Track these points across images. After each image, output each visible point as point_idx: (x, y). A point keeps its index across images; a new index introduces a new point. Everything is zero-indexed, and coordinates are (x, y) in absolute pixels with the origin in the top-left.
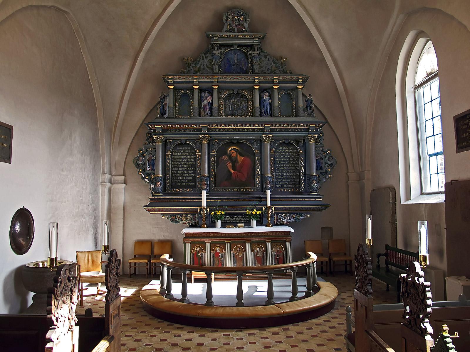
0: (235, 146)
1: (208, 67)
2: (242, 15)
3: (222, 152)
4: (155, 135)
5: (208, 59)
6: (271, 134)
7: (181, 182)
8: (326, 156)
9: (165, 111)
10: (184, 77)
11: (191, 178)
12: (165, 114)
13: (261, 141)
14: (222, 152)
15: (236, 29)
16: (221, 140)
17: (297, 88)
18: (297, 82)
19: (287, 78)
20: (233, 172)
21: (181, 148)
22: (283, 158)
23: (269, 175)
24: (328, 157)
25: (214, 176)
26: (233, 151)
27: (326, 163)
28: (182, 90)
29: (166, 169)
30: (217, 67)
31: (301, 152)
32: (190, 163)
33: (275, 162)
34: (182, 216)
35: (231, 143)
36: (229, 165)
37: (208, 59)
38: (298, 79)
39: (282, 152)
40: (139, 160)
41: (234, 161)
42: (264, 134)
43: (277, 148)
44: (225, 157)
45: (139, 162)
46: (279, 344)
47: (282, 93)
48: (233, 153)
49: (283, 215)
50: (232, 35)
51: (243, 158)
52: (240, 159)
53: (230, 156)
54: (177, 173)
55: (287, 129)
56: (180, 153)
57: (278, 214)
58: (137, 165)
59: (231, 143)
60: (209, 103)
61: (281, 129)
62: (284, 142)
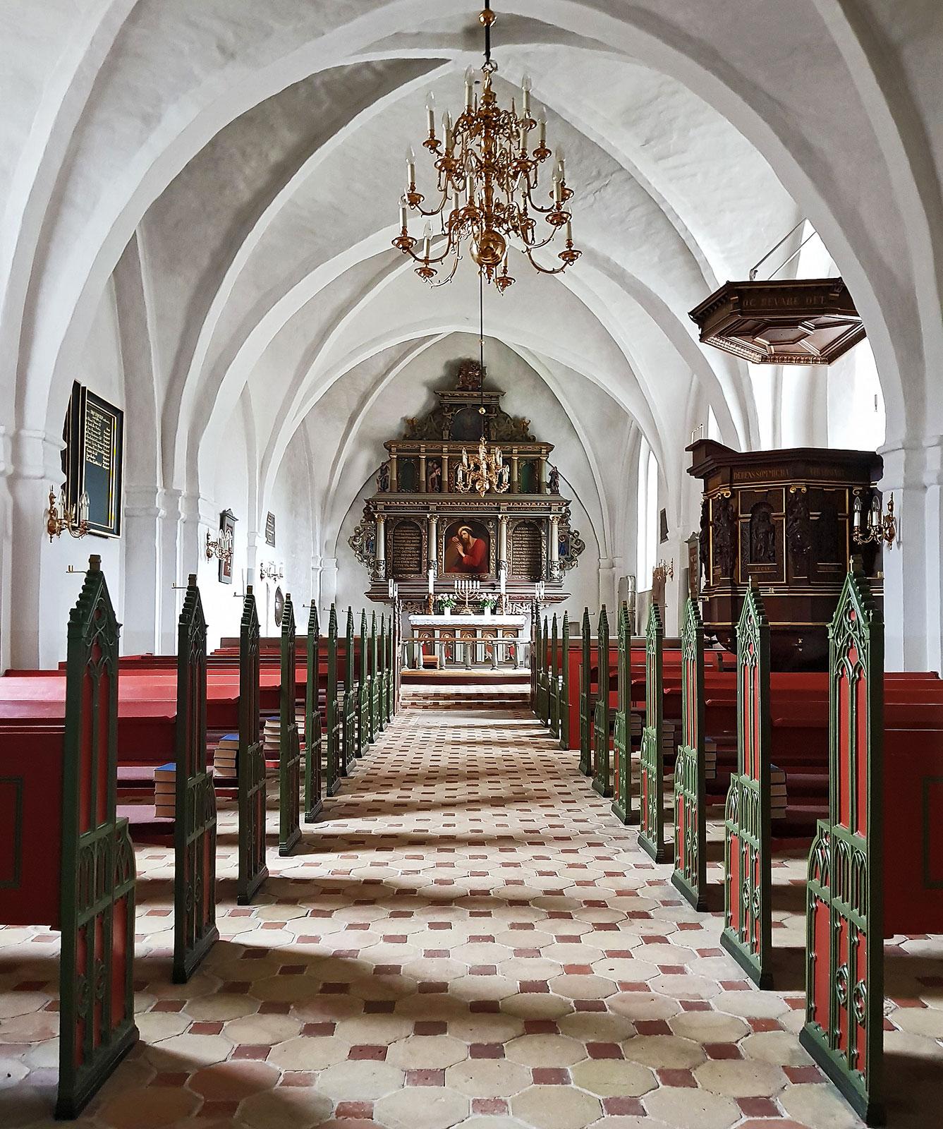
0: (467, 526)
1: (436, 431)
2: (477, 370)
3: (452, 532)
4: (377, 512)
5: (436, 421)
6: (436, 513)
7: (404, 567)
8: (573, 539)
9: (388, 485)
10: (408, 446)
11: (416, 562)
12: (387, 488)
13: (498, 522)
14: (452, 532)
15: (470, 387)
16: (450, 518)
17: (539, 459)
18: (540, 453)
19: (530, 448)
20: (464, 555)
21: (404, 527)
22: (522, 540)
23: (505, 560)
24: (574, 541)
25: (442, 560)
26: (464, 532)
27: (572, 547)
28: (405, 458)
29: (626, 800)
30: (448, 432)
31: (543, 533)
32: (414, 545)
33: (513, 545)
34: (407, 604)
35: (462, 522)
36: (460, 548)
37: (436, 421)
38: (541, 449)
39: (522, 534)
40: (355, 540)
41: (465, 543)
42: (499, 513)
43: (516, 529)
44: (455, 539)
45: (355, 543)
46: (672, 961)
47: (523, 464)
48: (464, 534)
49: (519, 605)
50: (466, 394)
51: (476, 539)
52: (472, 540)
53: (460, 537)
54: (400, 556)
55: (404, 507)
56: (403, 533)
57: (513, 604)
58: (353, 546)
59: (462, 522)
60: (437, 475)
61: (477, 507)
62: (524, 522)
